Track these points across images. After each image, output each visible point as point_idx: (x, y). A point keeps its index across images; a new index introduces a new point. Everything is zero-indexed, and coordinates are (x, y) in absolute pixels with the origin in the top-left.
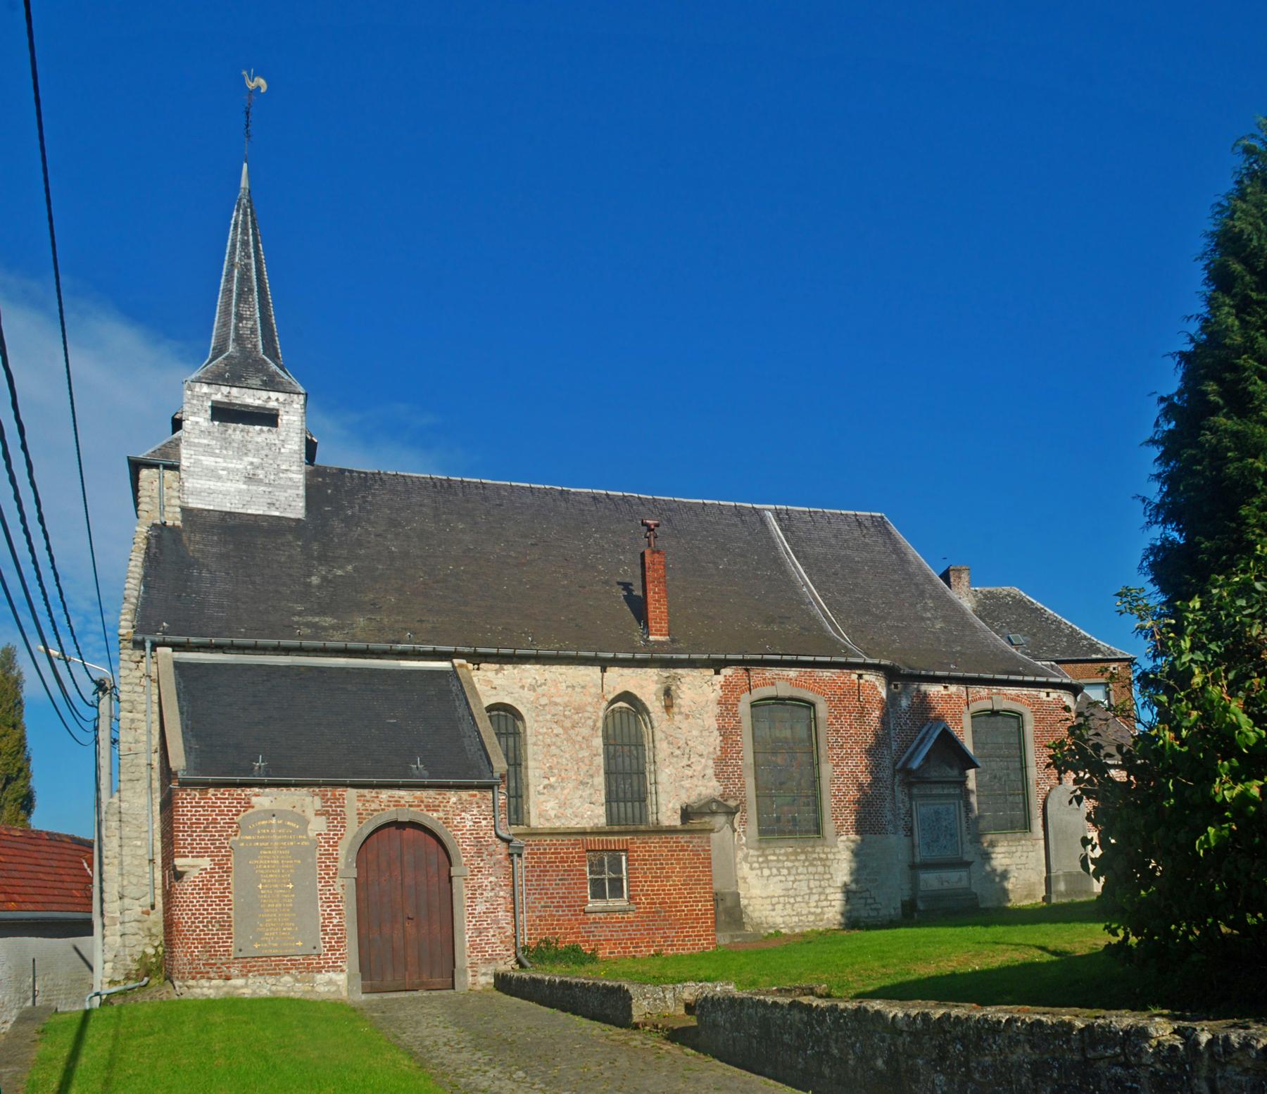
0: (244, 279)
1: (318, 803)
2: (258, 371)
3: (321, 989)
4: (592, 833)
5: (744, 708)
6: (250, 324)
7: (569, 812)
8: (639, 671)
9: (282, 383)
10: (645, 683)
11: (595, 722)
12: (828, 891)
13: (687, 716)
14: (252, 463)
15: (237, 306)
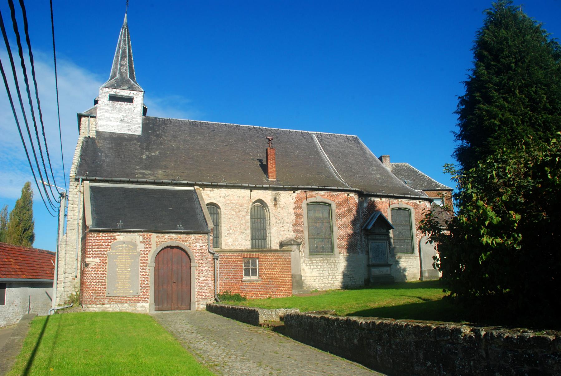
0: (124, 52)
1: (141, 238)
2: (127, 84)
3: (139, 309)
4: (245, 251)
5: (304, 205)
6: (125, 68)
8: (265, 191)
10: (267, 196)
11: (247, 210)
12: (336, 274)
13: (282, 208)
15: (121, 61)
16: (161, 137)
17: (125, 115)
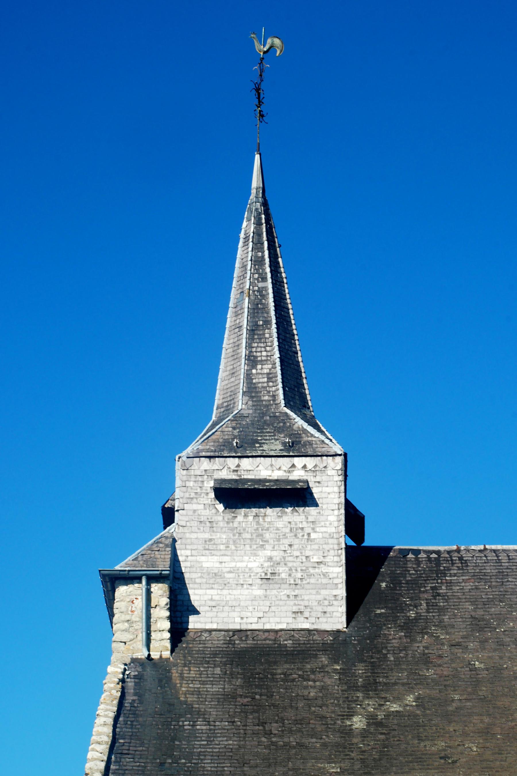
0: (257, 309)
2: (280, 430)
9: (310, 443)
14: (270, 559)
15: (249, 346)
16: (423, 633)
17: (277, 555)
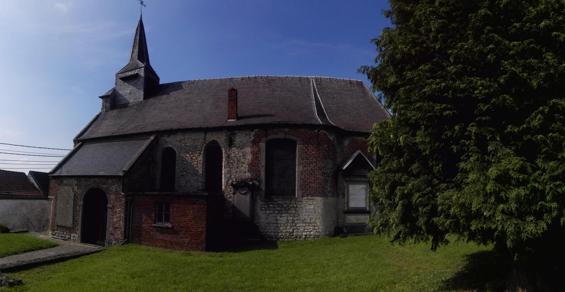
7: (189, 185)
12: (296, 222)
